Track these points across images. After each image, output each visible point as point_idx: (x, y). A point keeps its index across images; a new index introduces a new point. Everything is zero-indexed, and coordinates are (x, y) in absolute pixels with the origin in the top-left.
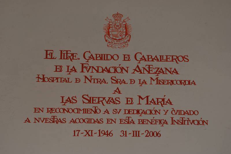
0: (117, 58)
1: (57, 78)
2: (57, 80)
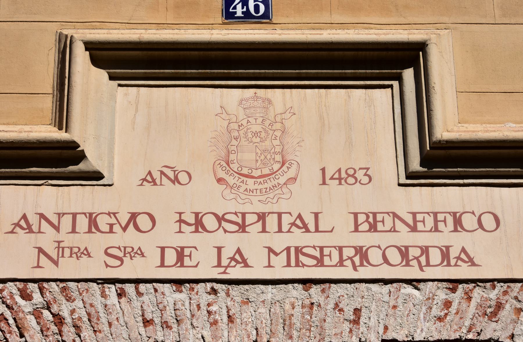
1: (262, 217)
2: (261, 222)
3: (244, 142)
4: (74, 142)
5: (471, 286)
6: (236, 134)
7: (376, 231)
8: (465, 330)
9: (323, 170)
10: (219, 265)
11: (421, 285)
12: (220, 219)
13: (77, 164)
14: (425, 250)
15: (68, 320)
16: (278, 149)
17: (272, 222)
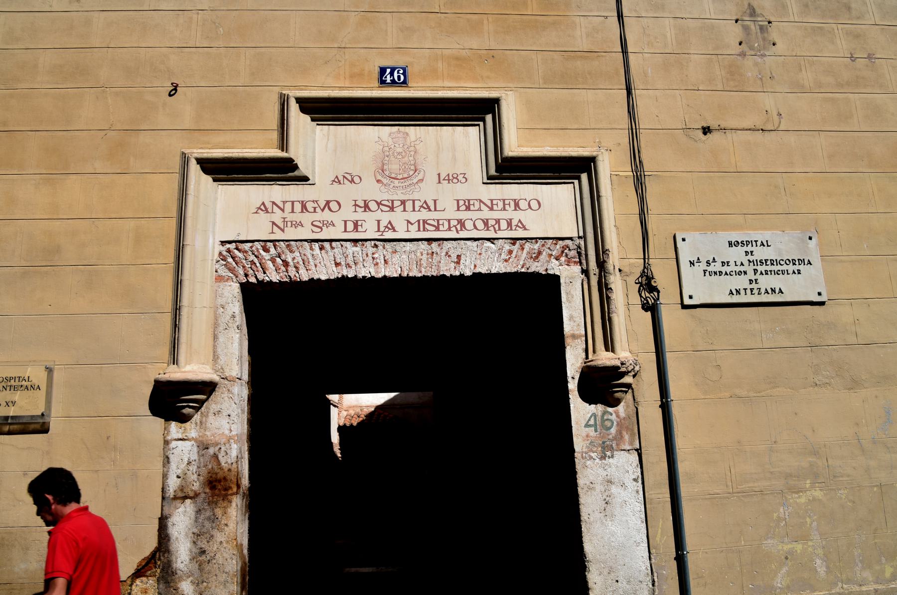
0: (537, 207)
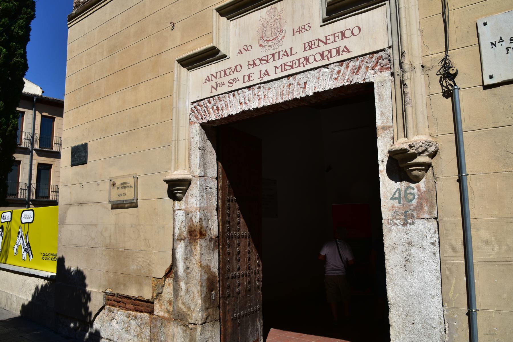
1: (273, 55)
3: (268, 28)
4: (214, 47)
5: (348, 62)
6: (265, 26)
7: (312, 48)
8: (345, 82)
9: (294, 30)
10: (260, 78)
11: (329, 67)
12: (260, 60)
13: (218, 54)
14: (330, 51)
15: (220, 108)
16: (279, 27)
17: (276, 56)
